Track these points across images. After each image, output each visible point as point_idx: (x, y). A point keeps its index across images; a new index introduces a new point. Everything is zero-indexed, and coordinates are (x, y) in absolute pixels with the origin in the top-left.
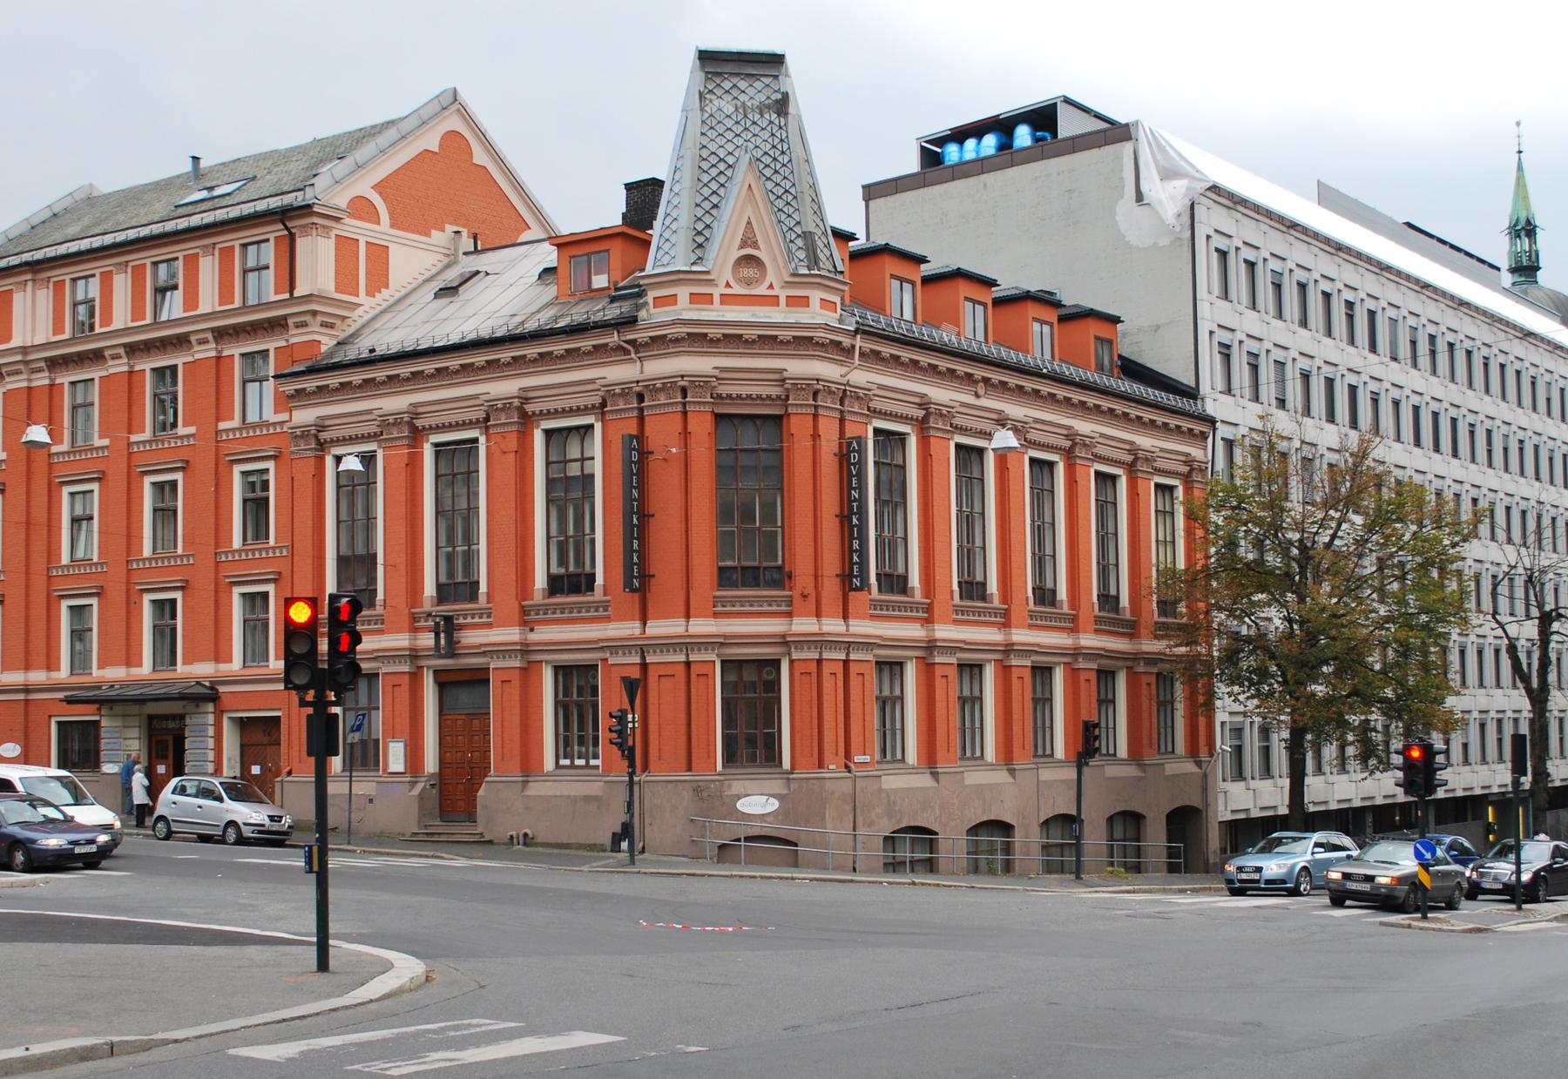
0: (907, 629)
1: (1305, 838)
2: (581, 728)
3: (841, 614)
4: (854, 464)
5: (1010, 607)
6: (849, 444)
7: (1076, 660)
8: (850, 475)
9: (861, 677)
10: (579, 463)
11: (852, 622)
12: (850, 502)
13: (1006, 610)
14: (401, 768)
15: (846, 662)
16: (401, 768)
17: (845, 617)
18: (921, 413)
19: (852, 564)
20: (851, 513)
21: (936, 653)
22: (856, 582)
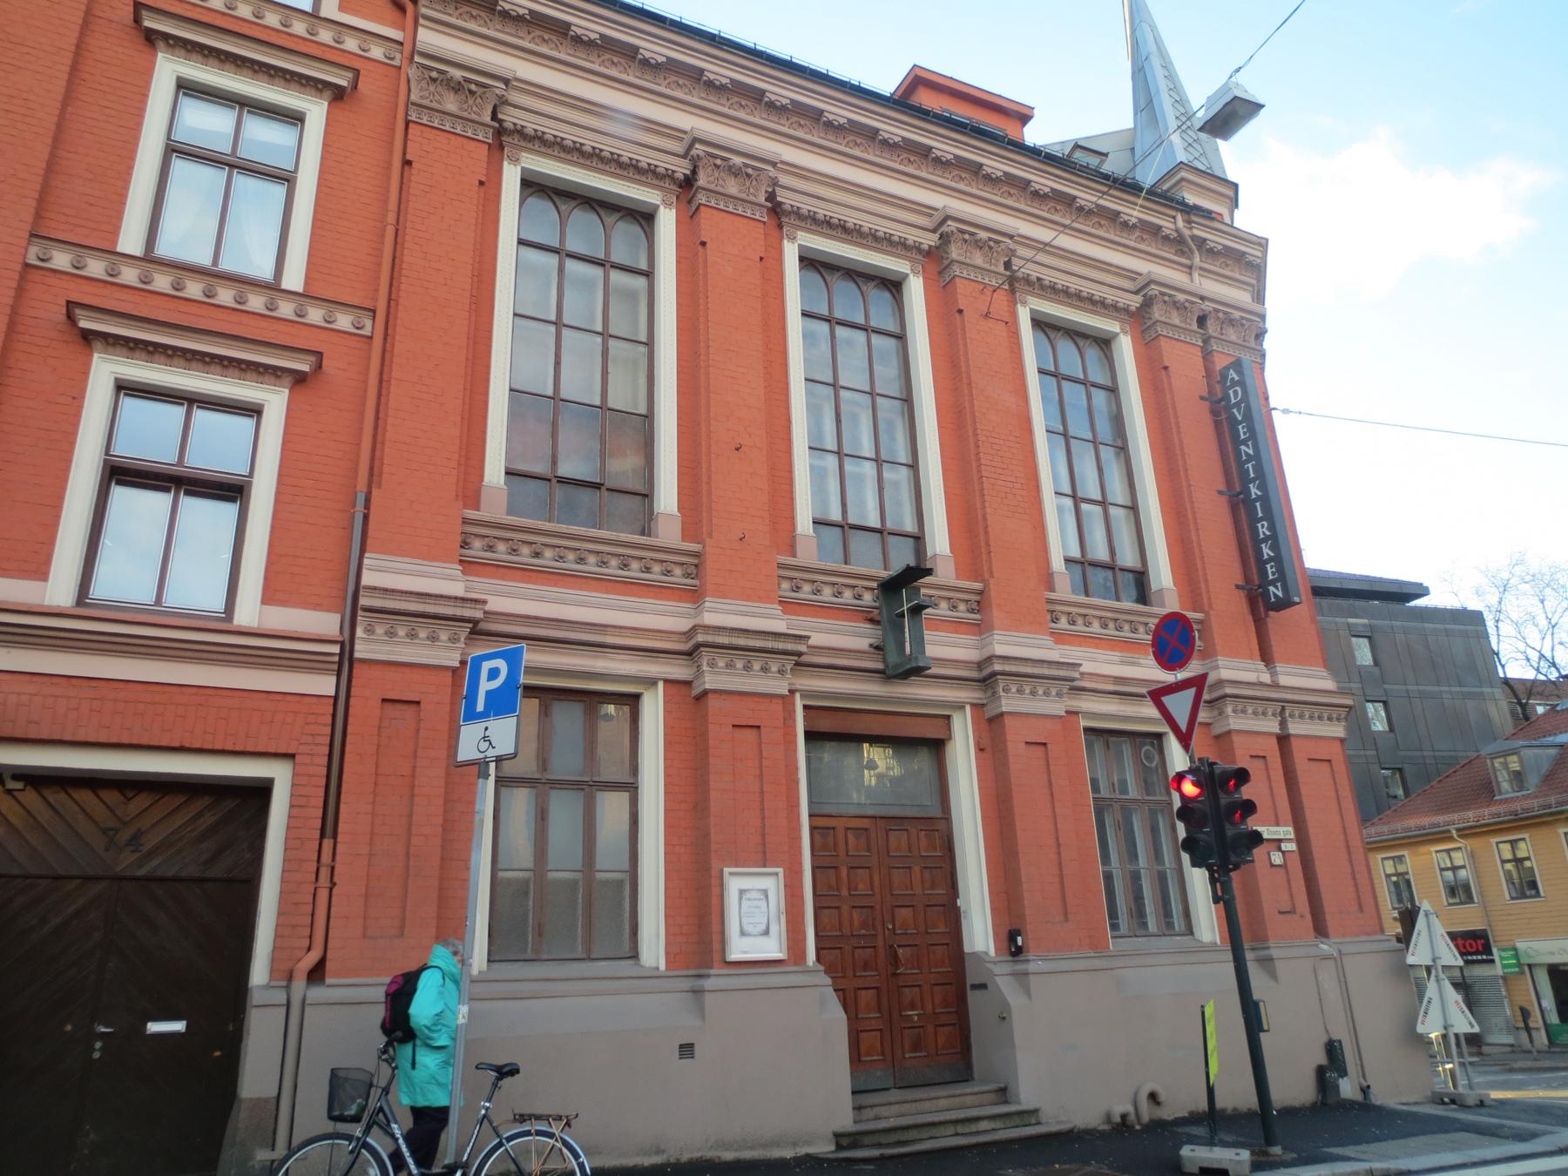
0: (1295, 675)
1: (1551, 1133)
2: (1136, 877)
3: (1257, 653)
4: (1237, 405)
5: (1207, 614)
6: (1224, 376)
7: (1221, 713)
8: (1234, 423)
9: (750, 735)
10: (565, 332)
11: (1280, 668)
12: (1241, 464)
13: (981, 593)
14: (772, 948)
15: (1283, 740)
16: (772, 948)
17: (1266, 657)
18: (1135, 302)
19: (1261, 563)
20: (1245, 481)
21: (1229, 710)
22: (1276, 591)
